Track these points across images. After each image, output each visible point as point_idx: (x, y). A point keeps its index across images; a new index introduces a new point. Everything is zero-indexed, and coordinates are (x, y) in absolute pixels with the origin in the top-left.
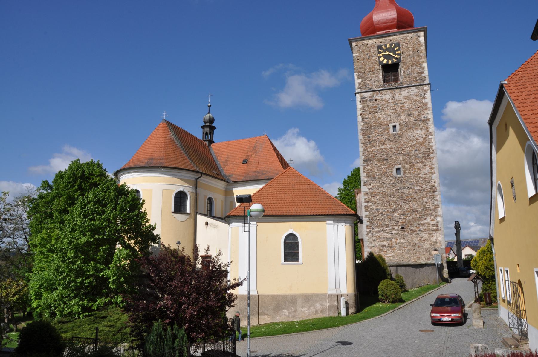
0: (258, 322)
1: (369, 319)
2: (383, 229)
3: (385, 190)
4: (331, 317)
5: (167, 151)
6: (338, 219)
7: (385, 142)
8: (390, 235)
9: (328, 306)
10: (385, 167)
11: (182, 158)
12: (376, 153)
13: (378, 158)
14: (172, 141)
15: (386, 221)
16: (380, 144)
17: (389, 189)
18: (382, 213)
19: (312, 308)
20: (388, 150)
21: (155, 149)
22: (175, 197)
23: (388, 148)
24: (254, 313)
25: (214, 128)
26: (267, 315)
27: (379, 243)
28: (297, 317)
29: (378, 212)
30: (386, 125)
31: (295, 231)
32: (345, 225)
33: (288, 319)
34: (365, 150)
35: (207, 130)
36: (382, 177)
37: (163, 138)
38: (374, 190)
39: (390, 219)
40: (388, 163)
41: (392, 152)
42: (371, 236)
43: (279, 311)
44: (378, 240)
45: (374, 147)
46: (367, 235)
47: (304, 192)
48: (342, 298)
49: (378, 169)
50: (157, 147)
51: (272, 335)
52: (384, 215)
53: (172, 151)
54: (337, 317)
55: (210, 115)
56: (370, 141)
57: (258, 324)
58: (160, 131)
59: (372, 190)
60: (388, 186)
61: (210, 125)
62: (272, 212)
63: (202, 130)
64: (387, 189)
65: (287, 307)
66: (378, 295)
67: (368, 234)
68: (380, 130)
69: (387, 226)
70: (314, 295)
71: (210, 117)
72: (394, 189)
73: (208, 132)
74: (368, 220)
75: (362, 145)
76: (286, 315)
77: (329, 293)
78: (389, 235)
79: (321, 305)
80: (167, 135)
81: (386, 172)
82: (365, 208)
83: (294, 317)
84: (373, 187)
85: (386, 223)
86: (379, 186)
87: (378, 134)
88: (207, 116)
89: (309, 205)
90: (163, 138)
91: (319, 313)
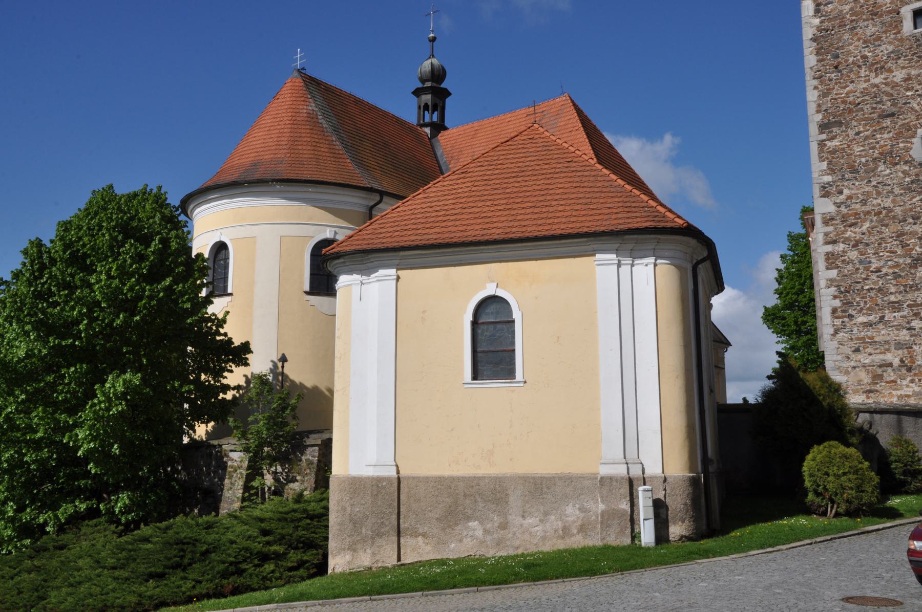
0: (395, 557)
2: (882, 317)
3: (888, 203)
4: (606, 548)
5: (296, 143)
6: (630, 246)
7: (886, 63)
8: (905, 332)
10: (886, 136)
11: (333, 159)
12: (859, 100)
13: (864, 115)
14: (313, 120)
15: (891, 293)
16: (871, 71)
17: (898, 199)
18: (878, 270)
20: (895, 85)
23: (895, 79)
24: (387, 529)
25: (446, 93)
26: (424, 535)
27: (871, 357)
28: (508, 543)
29: (865, 268)
30: (889, 12)
31: (504, 288)
32: (655, 265)
33: (483, 550)
34: (824, 97)
35: (427, 98)
36: (876, 168)
37: (290, 114)
38: (853, 206)
39: (905, 286)
40: (897, 123)
41: (908, 89)
42: (846, 339)
43: (456, 524)
44: (869, 350)
45: (852, 82)
46: (833, 335)
47: (549, 181)
48: (641, 488)
49: (862, 146)
50: (273, 136)
51: (389, 593)
52: (886, 275)
53: (310, 144)
54: (629, 546)
56: (840, 68)
57: (395, 563)
59: (847, 207)
60: (897, 191)
61: (435, 85)
64: (893, 201)
66: (805, 492)
67: (836, 332)
68: (871, 30)
69: (896, 306)
71: (432, 64)
72: (916, 197)
73: (430, 104)
74: (836, 293)
75: (816, 82)
77: (604, 471)
78: (902, 333)
79: (580, 509)
80: (301, 107)
81: (891, 152)
82: (827, 259)
83: (499, 543)
84: (850, 197)
85: (892, 298)
86: (868, 194)
87: (865, 42)
88: (426, 66)
89: (548, 212)
91: (573, 535)
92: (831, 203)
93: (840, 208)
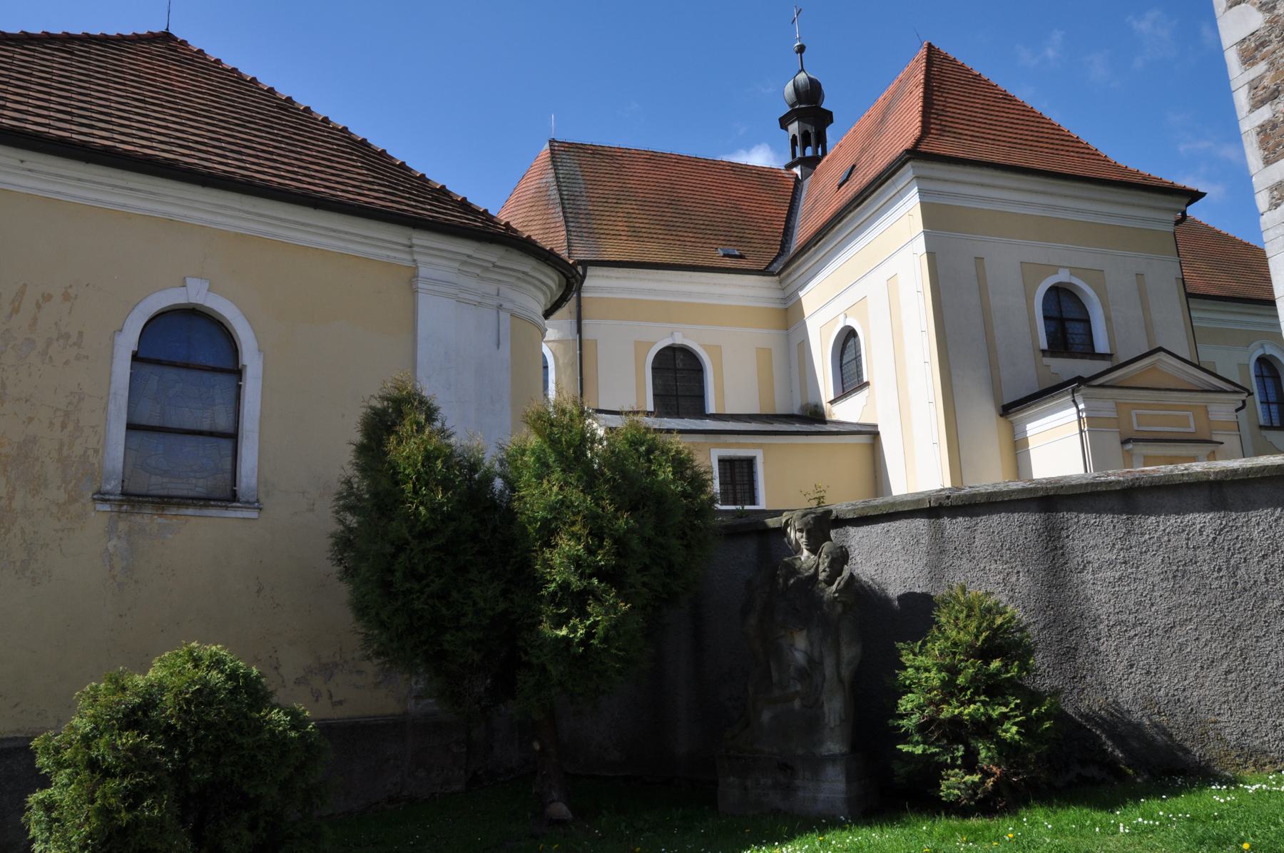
82: (1263, 144)
92: (1254, 10)
93: (1276, 12)
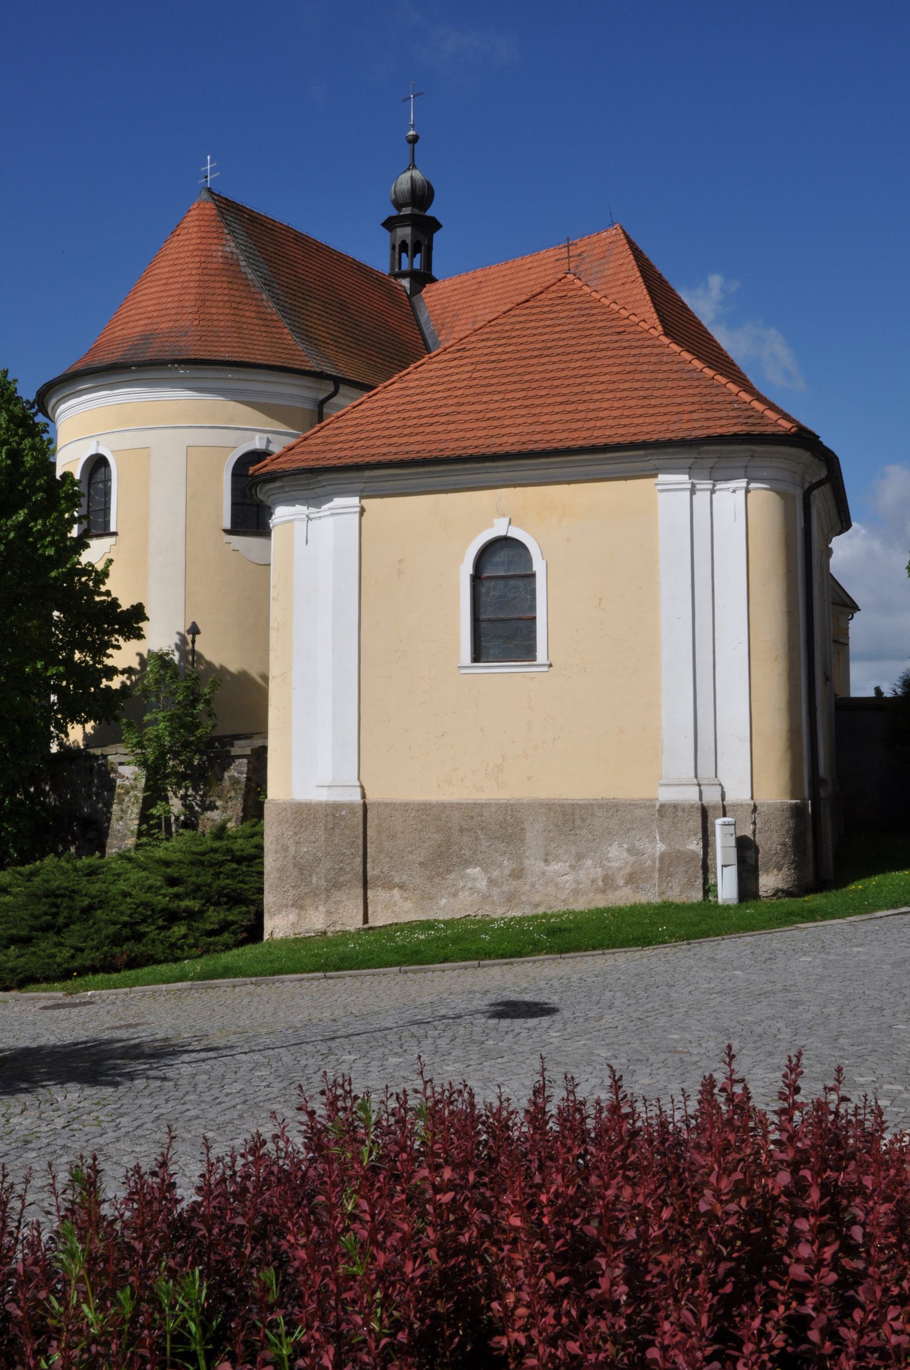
0: (360, 917)
1: (835, 918)
5: (208, 304)
6: (711, 462)
9: (658, 854)
11: (263, 329)
14: (233, 268)
19: (589, 862)
21: (164, 300)
22: (234, 475)
25: (434, 225)
26: (402, 887)
28: (524, 898)
31: (520, 526)
32: (747, 491)
33: (487, 908)
35: (405, 233)
37: (198, 259)
43: (449, 872)
48: (719, 821)
50: (172, 293)
51: (351, 969)
53: (228, 305)
54: (700, 904)
55: (417, 174)
57: (360, 925)
58: (188, 233)
61: (416, 211)
62: (423, 447)
63: (385, 233)
65: (480, 857)
70: (601, 806)
71: (412, 180)
76: (478, 892)
77: (666, 795)
79: (628, 850)
80: (213, 248)
83: (511, 898)
88: (404, 181)
90: (198, 259)
91: (618, 888)
